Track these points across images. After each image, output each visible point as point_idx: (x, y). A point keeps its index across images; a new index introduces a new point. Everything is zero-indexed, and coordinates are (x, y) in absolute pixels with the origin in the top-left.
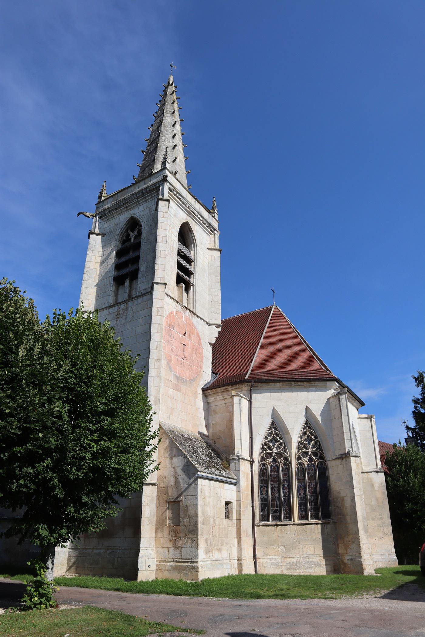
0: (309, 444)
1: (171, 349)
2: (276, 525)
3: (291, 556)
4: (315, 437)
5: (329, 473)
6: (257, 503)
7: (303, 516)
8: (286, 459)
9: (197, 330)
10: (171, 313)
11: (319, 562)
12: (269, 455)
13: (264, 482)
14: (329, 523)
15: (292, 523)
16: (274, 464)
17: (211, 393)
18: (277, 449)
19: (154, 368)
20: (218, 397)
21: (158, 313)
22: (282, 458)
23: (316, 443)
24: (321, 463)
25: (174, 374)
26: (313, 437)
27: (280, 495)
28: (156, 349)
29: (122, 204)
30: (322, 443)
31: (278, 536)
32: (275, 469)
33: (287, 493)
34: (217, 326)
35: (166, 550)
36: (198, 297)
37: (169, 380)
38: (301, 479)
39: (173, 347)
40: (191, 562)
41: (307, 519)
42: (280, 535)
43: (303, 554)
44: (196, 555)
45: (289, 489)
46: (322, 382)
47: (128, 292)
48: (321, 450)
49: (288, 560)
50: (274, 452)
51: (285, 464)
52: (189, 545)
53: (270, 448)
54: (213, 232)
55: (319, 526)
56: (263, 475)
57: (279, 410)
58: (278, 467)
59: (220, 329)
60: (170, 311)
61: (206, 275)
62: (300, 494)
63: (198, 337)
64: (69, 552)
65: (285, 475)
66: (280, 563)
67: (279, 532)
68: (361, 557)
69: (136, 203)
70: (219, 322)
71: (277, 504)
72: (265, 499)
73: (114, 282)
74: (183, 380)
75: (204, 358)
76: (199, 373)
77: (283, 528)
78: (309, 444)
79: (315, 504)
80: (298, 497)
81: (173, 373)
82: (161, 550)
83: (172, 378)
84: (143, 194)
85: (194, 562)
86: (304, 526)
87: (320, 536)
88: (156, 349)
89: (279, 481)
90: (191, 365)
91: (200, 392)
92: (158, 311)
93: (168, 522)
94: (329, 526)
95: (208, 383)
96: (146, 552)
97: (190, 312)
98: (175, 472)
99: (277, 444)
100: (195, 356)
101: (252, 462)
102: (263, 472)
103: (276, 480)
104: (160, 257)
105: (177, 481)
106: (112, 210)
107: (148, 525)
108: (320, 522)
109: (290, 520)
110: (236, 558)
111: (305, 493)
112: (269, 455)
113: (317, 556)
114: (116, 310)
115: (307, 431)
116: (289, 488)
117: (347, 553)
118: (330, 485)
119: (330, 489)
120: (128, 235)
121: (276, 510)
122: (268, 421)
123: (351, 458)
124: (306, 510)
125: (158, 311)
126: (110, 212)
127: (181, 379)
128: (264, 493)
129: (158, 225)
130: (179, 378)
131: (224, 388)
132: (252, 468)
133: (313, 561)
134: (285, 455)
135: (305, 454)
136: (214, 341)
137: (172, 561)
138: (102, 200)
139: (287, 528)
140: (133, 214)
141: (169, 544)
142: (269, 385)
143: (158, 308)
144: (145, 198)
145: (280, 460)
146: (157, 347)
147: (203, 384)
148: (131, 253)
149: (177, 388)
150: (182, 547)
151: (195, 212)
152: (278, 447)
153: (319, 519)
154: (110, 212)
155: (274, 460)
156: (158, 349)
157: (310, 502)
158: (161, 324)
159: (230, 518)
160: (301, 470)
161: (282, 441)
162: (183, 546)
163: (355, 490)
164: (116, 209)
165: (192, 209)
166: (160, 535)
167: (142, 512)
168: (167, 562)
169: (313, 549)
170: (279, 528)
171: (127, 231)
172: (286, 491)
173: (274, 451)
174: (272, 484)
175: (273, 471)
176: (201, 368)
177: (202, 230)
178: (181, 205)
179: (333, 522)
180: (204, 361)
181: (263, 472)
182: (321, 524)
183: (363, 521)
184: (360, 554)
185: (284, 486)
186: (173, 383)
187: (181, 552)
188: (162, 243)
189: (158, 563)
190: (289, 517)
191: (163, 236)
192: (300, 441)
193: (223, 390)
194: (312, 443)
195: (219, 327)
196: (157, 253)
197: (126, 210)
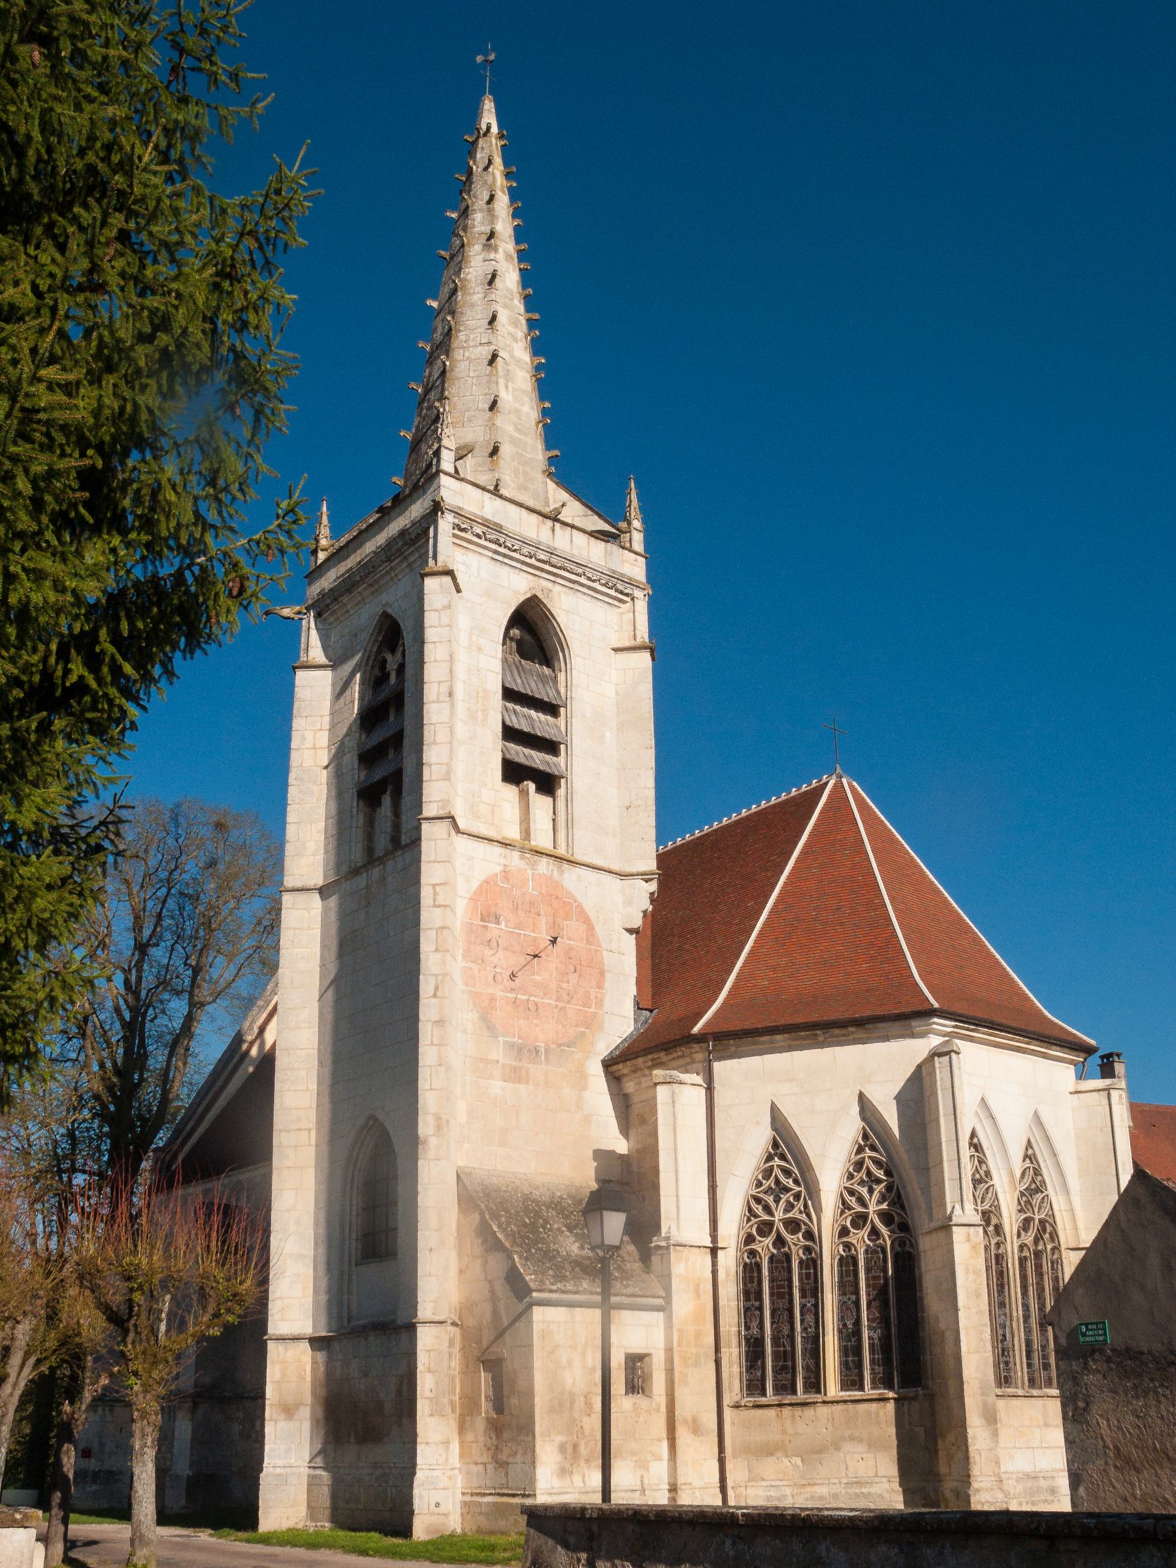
0: (871, 1191)
1: (491, 978)
2: (780, 1405)
3: (818, 1482)
4: (888, 1173)
5: (919, 1268)
6: (733, 1355)
7: (851, 1378)
8: (809, 1235)
9: (580, 905)
10: (487, 882)
11: (887, 1495)
12: (765, 1228)
13: (752, 1296)
14: (915, 1398)
15: (819, 1398)
16: (779, 1249)
17: (625, 1071)
18: (786, 1211)
19: (432, 1044)
20: (643, 1080)
21: (435, 900)
22: (800, 1235)
23: (889, 1188)
24: (899, 1243)
25: (505, 1042)
26: (880, 1174)
27: (792, 1329)
28: (435, 996)
29: (358, 578)
30: (904, 1187)
31: (784, 1432)
32: (781, 1263)
33: (812, 1324)
34: (646, 877)
35: (481, 1467)
36: (579, 810)
37: (488, 1062)
38: (848, 1285)
39: (498, 970)
40: (524, 1496)
41: (862, 1388)
42: (790, 1431)
43: (847, 1476)
44: (532, 1481)
45: (816, 1314)
46: (897, 1024)
47: (389, 830)
48: (903, 1207)
49: (809, 1489)
50: (776, 1219)
51: (807, 1250)
52: (519, 1458)
53: (767, 1209)
54: (627, 595)
55: (890, 1406)
56: (752, 1281)
57: (785, 1109)
58: (788, 1257)
59: (653, 886)
60: (483, 878)
61: (608, 734)
62: (845, 1325)
63: (584, 923)
64: (309, 1476)
65: (808, 1276)
66: (790, 1497)
67: (788, 1423)
68: (969, 1484)
69: (388, 572)
70: (651, 865)
71: (785, 1352)
72: (756, 1339)
73: (361, 802)
74: (537, 1052)
75: (608, 975)
76: (591, 1023)
77: (798, 1411)
78: (871, 1191)
79: (883, 1348)
80: (840, 1331)
81: (501, 1039)
82: (474, 1468)
83: (498, 1053)
84: (398, 550)
85: (529, 1496)
86: (850, 1406)
87: (892, 1431)
88: (435, 996)
89: (791, 1294)
90: (561, 1004)
91: (596, 1070)
92: (435, 894)
93: (484, 1405)
94: (916, 1406)
95: (618, 1047)
96: (429, 1473)
97: (551, 861)
98: (492, 1292)
99: (784, 1198)
100: (573, 978)
101: (714, 1251)
102: (750, 1272)
103: (782, 1291)
104: (435, 743)
105: (495, 1313)
106: (341, 595)
107: (431, 1415)
108: (891, 1394)
109: (818, 1391)
110: (667, 1487)
111: (858, 1322)
112: (765, 1228)
113: (884, 1480)
114: (364, 884)
115: (864, 1158)
116: (815, 1311)
117: (950, 1475)
118: (922, 1299)
119: (923, 1311)
120: (384, 662)
121: (784, 1368)
122: (762, 1136)
123: (954, 1228)
124: (859, 1365)
125: (435, 894)
126: (336, 600)
127: (529, 1050)
128: (754, 1324)
129: (426, 652)
130: (525, 1051)
131: (650, 1057)
132: (714, 1264)
133: (869, 1494)
134: (805, 1224)
135: (860, 1220)
136: (637, 922)
137: (491, 1494)
138: (319, 562)
139: (809, 1412)
140: (387, 604)
141: (486, 1458)
142: (756, 1043)
143: (434, 885)
144: (406, 558)
145: (795, 1240)
146: (436, 989)
147: (608, 1047)
148: (392, 718)
149: (515, 1075)
150: (508, 1464)
151: (554, 560)
152: (790, 1207)
153: (890, 1387)
154: (336, 600)
155: (780, 1241)
156: (439, 994)
157: (872, 1346)
158: (444, 928)
159: (647, 1393)
160: (847, 1264)
161: (799, 1189)
162: (511, 1460)
163: (960, 1313)
164: (349, 591)
165: (542, 557)
166: (470, 1437)
167: (418, 1388)
168: (484, 1495)
169: (871, 1462)
170: (787, 1411)
171: (379, 652)
172: (810, 1318)
173: (779, 1215)
174: (772, 1302)
175: (777, 1268)
176: (600, 1003)
177: (589, 599)
178: (505, 556)
179: (924, 1395)
180: (607, 985)
181: (751, 1271)
182: (895, 1399)
183: (983, 1394)
184: (969, 1476)
185: (803, 1307)
186: (503, 1064)
187: (507, 1474)
188: (438, 701)
189: (468, 1498)
190: (815, 1383)
191: (439, 683)
192: (847, 1185)
193: (650, 1063)
194: (879, 1188)
195: (652, 879)
196: (426, 733)
197: (372, 593)
